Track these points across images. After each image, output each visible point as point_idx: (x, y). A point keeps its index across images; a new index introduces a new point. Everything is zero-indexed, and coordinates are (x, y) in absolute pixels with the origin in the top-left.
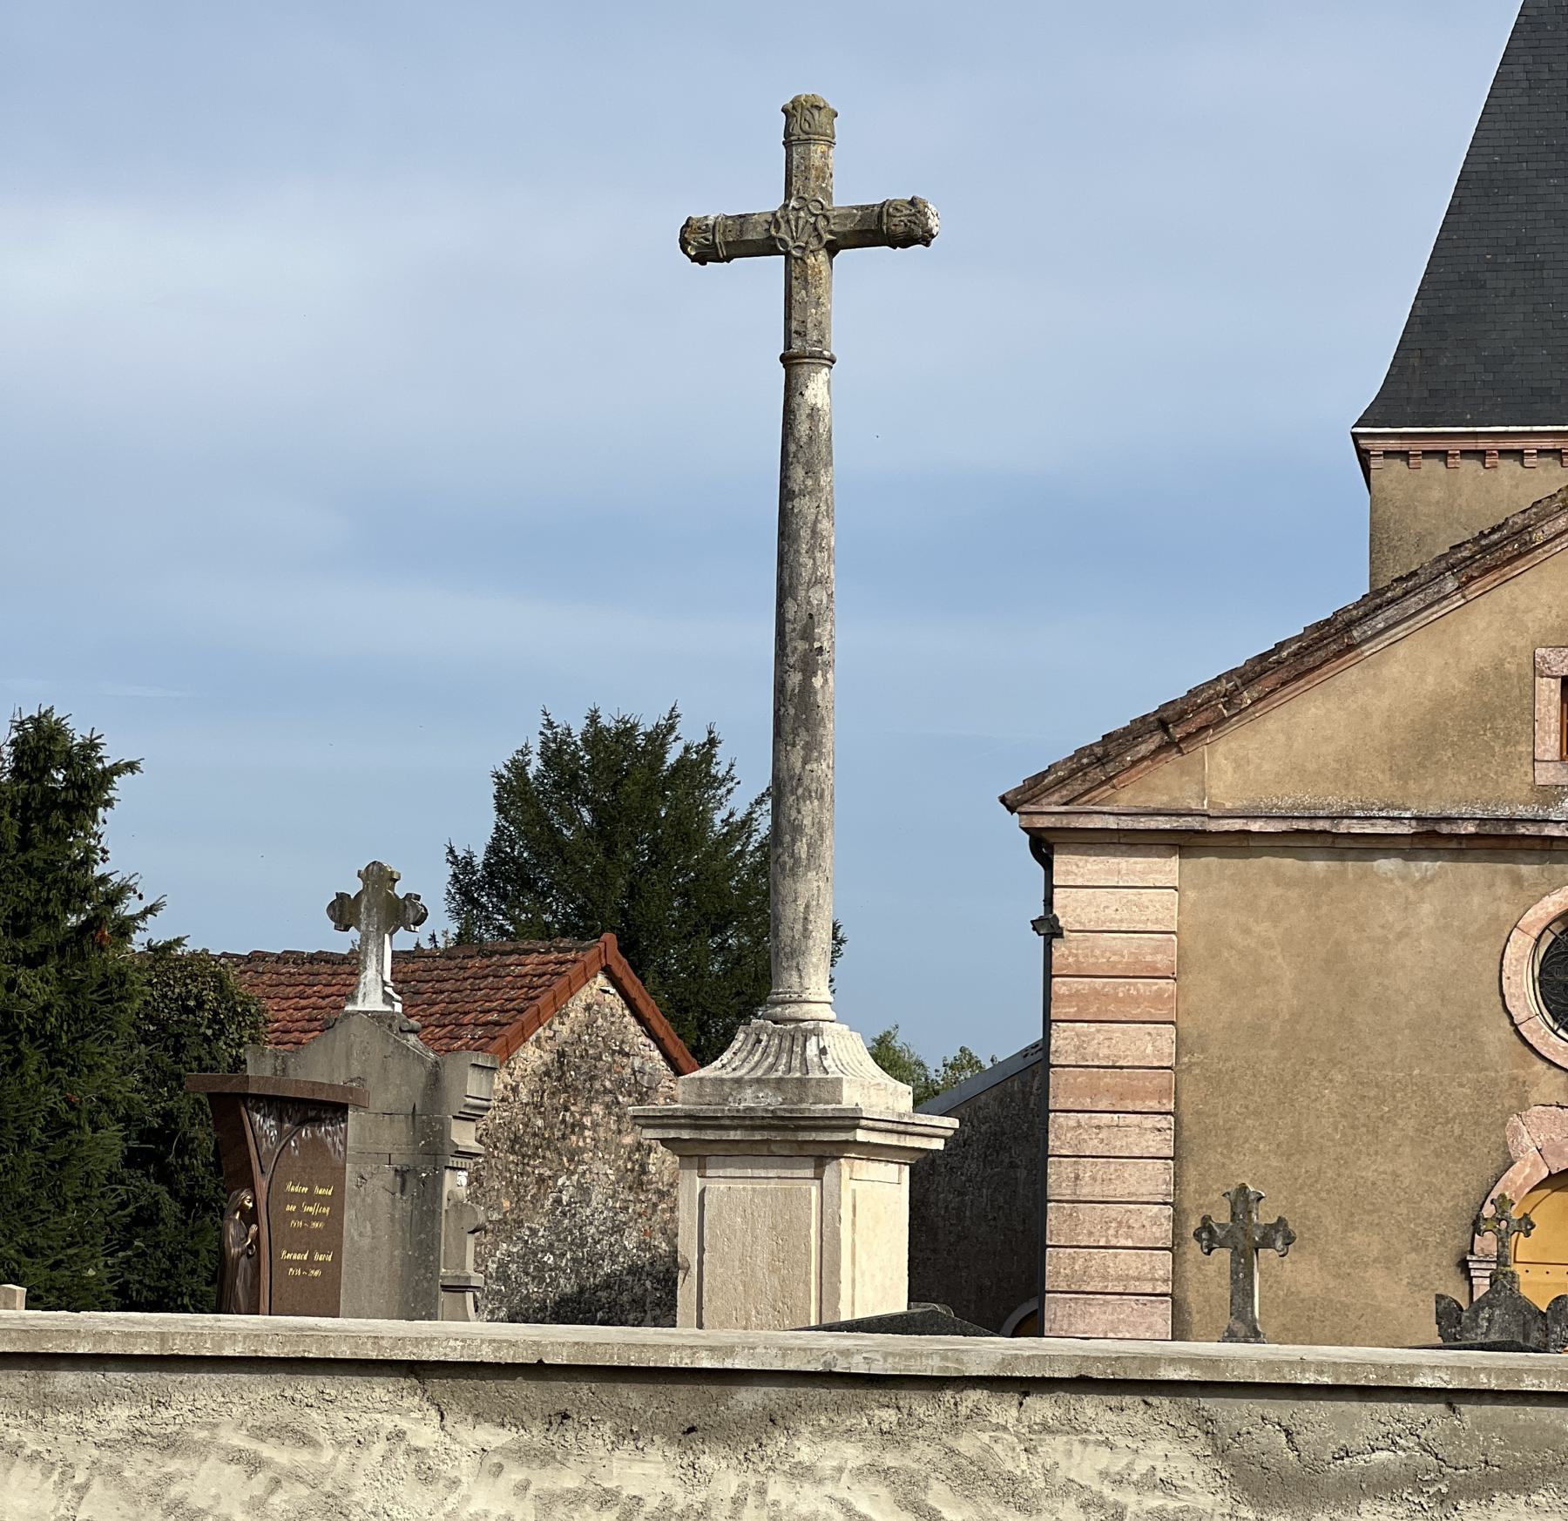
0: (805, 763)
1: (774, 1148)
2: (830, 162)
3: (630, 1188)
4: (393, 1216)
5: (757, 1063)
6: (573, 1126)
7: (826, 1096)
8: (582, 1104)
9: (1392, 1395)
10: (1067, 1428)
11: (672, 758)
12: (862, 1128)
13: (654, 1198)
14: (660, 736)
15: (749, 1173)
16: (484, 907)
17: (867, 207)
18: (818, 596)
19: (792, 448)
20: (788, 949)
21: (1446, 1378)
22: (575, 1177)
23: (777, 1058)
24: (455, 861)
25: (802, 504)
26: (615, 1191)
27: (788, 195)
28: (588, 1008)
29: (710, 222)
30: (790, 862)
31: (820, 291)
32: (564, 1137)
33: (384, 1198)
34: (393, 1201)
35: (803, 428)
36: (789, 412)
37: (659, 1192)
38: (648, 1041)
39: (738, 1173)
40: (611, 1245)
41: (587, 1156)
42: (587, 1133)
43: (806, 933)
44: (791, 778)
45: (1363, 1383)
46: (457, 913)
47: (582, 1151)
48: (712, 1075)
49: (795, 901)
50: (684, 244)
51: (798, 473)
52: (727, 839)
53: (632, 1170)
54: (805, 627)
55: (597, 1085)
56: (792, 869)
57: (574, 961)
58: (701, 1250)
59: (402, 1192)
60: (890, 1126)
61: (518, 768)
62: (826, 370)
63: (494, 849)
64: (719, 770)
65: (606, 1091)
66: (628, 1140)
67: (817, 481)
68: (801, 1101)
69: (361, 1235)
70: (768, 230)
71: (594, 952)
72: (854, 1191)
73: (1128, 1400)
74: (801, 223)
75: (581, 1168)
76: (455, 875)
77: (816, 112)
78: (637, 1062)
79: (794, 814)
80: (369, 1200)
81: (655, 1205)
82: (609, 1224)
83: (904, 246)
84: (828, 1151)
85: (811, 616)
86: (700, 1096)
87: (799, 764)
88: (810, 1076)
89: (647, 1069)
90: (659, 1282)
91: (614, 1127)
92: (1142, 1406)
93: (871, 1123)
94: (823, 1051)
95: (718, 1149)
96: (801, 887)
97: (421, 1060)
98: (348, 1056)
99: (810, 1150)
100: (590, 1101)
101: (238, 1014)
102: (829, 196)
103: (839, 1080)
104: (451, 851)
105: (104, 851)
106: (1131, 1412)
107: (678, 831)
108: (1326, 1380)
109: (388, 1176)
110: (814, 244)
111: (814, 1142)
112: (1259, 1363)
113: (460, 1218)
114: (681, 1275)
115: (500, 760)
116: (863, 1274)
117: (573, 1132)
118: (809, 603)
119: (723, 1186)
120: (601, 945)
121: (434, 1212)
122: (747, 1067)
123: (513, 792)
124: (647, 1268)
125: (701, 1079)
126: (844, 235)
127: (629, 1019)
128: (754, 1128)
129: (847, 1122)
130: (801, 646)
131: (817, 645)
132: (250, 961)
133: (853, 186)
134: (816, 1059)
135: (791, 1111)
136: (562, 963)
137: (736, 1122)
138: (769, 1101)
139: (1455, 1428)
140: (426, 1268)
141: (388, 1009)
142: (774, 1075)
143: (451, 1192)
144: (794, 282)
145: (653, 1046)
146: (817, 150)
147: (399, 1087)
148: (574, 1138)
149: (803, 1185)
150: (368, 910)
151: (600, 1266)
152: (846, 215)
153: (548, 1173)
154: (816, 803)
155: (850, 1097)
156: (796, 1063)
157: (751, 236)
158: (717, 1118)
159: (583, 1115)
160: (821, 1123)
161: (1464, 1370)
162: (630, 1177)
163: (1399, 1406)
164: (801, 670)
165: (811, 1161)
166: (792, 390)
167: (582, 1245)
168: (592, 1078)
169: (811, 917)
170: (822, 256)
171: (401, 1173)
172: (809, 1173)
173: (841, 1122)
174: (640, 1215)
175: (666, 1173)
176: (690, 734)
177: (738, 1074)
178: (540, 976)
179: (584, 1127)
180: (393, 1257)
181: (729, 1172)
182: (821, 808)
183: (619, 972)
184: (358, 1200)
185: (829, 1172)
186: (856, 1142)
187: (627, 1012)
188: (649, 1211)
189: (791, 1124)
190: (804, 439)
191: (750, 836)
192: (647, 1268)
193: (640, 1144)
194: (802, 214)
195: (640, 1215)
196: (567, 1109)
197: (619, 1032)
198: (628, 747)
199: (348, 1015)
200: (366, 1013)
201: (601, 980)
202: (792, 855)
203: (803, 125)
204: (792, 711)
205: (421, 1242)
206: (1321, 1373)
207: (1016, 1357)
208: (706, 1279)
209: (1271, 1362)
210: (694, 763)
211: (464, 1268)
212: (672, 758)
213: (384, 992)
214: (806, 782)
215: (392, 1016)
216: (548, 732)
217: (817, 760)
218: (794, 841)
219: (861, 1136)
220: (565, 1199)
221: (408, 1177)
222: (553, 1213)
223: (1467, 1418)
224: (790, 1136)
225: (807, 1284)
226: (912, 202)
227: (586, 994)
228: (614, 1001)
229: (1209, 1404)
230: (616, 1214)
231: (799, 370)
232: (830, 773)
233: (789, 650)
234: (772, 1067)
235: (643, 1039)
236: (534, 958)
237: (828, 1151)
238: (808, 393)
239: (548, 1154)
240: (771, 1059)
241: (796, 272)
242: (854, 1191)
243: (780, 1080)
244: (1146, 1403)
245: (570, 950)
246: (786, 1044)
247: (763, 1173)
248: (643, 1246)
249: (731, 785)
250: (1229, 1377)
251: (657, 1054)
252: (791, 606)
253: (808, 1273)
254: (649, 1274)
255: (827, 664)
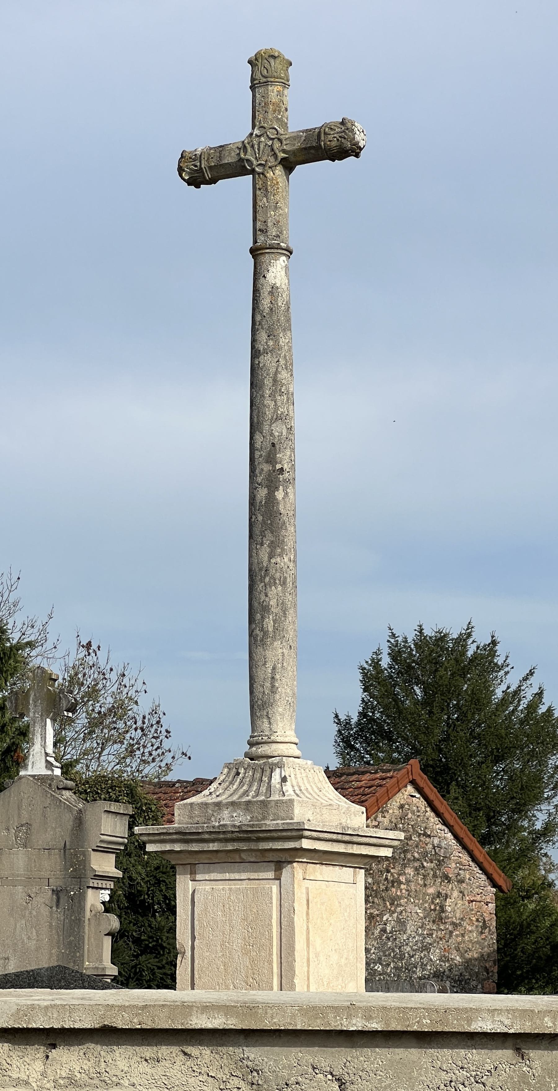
0: (270, 557)
1: (244, 856)
2: (285, 99)
3: (434, 922)
4: (51, 924)
5: (235, 791)
6: (393, 882)
7: (282, 814)
8: (398, 868)
9: (454, 1041)
10: (96, 1081)
11: (470, 653)
12: (307, 838)
13: (451, 928)
14: (463, 640)
15: (227, 876)
16: (358, 750)
17: (310, 130)
18: (279, 429)
19: (258, 318)
20: (260, 702)
21: (507, 1022)
22: (395, 915)
23: (250, 786)
24: (339, 723)
25: (267, 360)
26: (423, 924)
27: (254, 127)
28: (402, 807)
29: (198, 153)
30: (260, 634)
31: (277, 197)
32: (387, 889)
33: (45, 911)
34: (51, 913)
35: (265, 303)
36: (256, 291)
37: (453, 924)
38: (443, 827)
39: (219, 876)
40: (421, 958)
41: (403, 901)
42: (402, 886)
43: (273, 690)
44: (261, 570)
45: (415, 1028)
46: (342, 754)
47: (400, 898)
48: (200, 801)
49: (265, 664)
50: (180, 170)
51: (263, 336)
52: (504, 702)
53: (435, 910)
54: (269, 453)
55: (409, 856)
56: (262, 640)
57: (391, 777)
58: (193, 938)
59: (57, 906)
60: (335, 837)
61: (376, 663)
62: (284, 258)
63: (363, 714)
64: (499, 660)
65: (415, 860)
66: (431, 890)
67: (277, 341)
68: (264, 818)
69: (29, 938)
70: (239, 154)
71: (404, 771)
72: (307, 889)
73: (164, 1051)
74: (262, 146)
75: (399, 909)
76: (339, 731)
77: (272, 61)
78: (436, 841)
79: (263, 597)
80: (34, 913)
81: (451, 932)
82: (419, 945)
83: (340, 159)
84: (283, 857)
85: (273, 445)
86: (191, 817)
87: (266, 559)
88: (272, 798)
89: (443, 845)
90: (455, 982)
91: (421, 882)
92: (182, 1057)
93: (315, 834)
94: (284, 780)
95: (203, 858)
96: (269, 654)
97: (69, 809)
98: (19, 808)
99: (271, 856)
100: (404, 866)
101: (144, 812)
102: (285, 126)
103: (291, 801)
104: (337, 716)
105: (168, 732)
106: (167, 1064)
107: (473, 698)
108: (375, 1026)
109: (48, 894)
110: (272, 162)
111: (271, 850)
112: (301, 1009)
113: (99, 924)
114: (179, 958)
115: (365, 657)
116: (317, 955)
117: (393, 886)
118: (272, 434)
119: (207, 887)
120: (409, 767)
121: (80, 920)
122: (228, 793)
123: (372, 678)
124: (447, 973)
125: (191, 804)
126: (294, 153)
127: (430, 814)
128: (227, 840)
129: (294, 834)
130: (266, 467)
131: (278, 466)
132: (194, 784)
133: (302, 113)
134: (278, 786)
135: (252, 826)
136: (384, 779)
137: (213, 836)
138: (240, 819)
139: (524, 1075)
140: (74, 962)
141: (49, 773)
142: (246, 799)
143: (92, 905)
144: (258, 192)
145: (446, 830)
146: (273, 91)
147: (54, 829)
148: (394, 890)
149: (266, 884)
150: (35, 702)
151: (414, 972)
152: (296, 137)
153: (377, 912)
154: (280, 588)
155: (301, 814)
156: (263, 789)
157: (228, 160)
158: (199, 833)
159: (400, 875)
160: (275, 834)
161: (526, 1013)
162: (433, 914)
163: (463, 1052)
164: (267, 486)
165: (272, 866)
166: (258, 274)
167: (401, 959)
168: (405, 852)
169: (277, 677)
170: (279, 171)
171: (56, 892)
172: (271, 875)
173: (289, 834)
174: (441, 939)
175: (458, 911)
176: (481, 638)
177: (219, 799)
178: (370, 787)
179: (400, 883)
180: (51, 954)
181: (214, 876)
182: (284, 592)
183: (421, 784)
184: (27, 912)
185: (286, 873)
186: (302, 849)
187: (428, 809)
188: (447, 936)
189: (253, 836)
190: (267, 310)
191: (519, 701)
192: (447, 973)
193: (439, 893)
194: (262, 139)
195: (441, 939)
196: (388, 871)
197: (423, 821)
198: (442, 649)
199: (21, 778)
200: (33, 776)
201: (410, 789)
202: (262, 629)
203: (265, 72)
204: (260, 518)
205: (70, 943)
206: (369, 1018)
207: (33, 1007)
208: (196, 962)
209: (314, 1008)
210: (482, 656)
211: (101, 961)
212: (470, 653)
213: (47, 761)
214: (272, 571)
215: (52, 778)
216: (392, 641)
217: (281, 555)
218: (263, 618)
219: (306, 844)
220: (389, 929)
221: (62, 895)
222: (381, 938)
223: (537, 1064)
224: (253, 846)
225: (270, 963)
226: (343, 123)
227: (400, 798)
228: (420, 802)
229: (254, 1054)
230: (424, 938)
231: (262, 258)
232: (291, 565)
233: (257, 471)
234: (246, 793)
235: (440, 826)
236: (367, 776)
237: (283, 857)
238: (270, 276)
239: (376, 900)
240: (245, 788)
241: (260, 184)
242: (307, 889)
243: (249, 802)
244: (185, 1054)
245: (390, 771)
246: (258, 775)
247: (236, 876)
248: (444, 958)
249: (506, 669)
250: (267, 1024)
251: (449, 835)
252: (258, 437)
253: (271, 954)
254: (448, 977)
255: (287, 481)
